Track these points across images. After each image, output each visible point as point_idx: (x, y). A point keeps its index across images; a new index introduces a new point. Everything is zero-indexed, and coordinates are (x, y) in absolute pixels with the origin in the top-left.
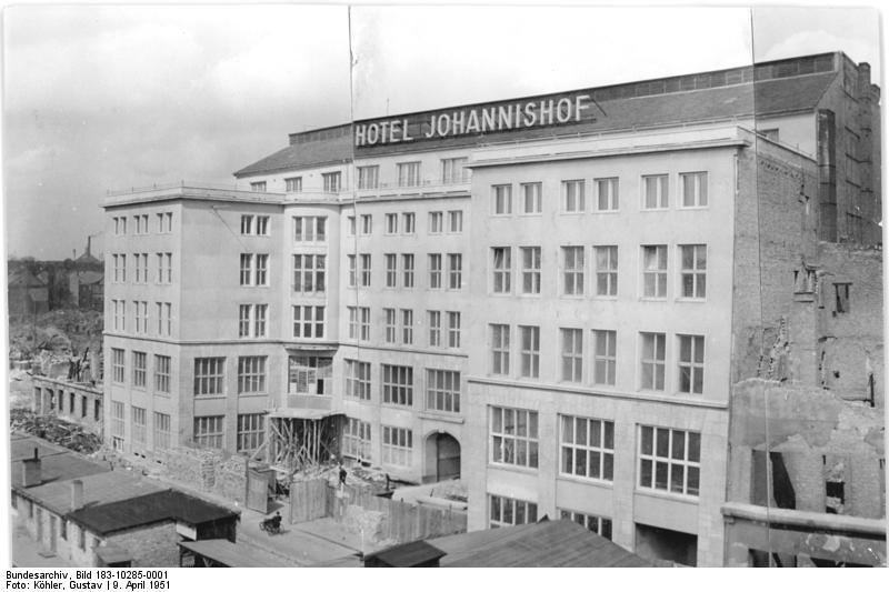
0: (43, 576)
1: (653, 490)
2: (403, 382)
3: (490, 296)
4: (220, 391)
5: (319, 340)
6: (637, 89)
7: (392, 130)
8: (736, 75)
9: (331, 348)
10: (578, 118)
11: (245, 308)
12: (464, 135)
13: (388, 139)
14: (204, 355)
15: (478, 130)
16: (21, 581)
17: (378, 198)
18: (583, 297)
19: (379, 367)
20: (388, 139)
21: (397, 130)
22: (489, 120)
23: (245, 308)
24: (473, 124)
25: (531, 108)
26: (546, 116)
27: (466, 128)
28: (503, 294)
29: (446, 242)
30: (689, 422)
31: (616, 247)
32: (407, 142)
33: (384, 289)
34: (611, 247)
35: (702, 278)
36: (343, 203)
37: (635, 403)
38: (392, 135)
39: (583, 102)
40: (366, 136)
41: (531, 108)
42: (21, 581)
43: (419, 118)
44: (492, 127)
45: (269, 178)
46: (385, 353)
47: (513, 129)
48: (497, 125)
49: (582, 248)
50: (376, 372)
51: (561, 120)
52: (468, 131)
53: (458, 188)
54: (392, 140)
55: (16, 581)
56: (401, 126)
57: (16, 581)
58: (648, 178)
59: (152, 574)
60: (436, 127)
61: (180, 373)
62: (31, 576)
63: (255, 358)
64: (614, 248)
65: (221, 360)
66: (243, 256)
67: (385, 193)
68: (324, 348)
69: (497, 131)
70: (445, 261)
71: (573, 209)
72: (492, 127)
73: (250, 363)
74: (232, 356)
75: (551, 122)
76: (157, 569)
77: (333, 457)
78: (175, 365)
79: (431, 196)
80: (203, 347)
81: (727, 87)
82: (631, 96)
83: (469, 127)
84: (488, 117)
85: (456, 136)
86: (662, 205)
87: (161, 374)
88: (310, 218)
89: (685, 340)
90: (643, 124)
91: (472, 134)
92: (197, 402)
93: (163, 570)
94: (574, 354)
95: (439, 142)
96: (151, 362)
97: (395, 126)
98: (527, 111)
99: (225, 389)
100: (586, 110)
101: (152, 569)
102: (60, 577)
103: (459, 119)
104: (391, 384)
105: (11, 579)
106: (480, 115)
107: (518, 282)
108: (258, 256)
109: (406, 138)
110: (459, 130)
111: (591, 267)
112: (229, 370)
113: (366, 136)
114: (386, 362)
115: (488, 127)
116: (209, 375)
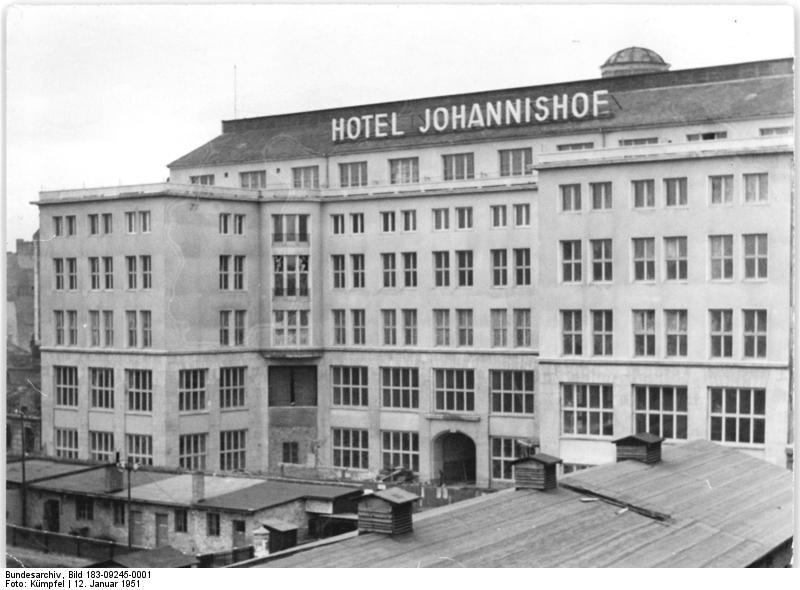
0: (39, 576)
1: (723, 443)
2: (144, 387)
3: (591, 285)
4: (203, 407)
5: (304, 347)
6: (741, 72)
7: (378, 124)
8: (751, 70)
9: (316, 355)
10: (596, 113)
11: (225, 313)
12: (467, 131)
13: (373, 132)
14: (188, 367)
15: (482, 124)
16: (19, 580)
17: (480, 189)
18: (655, 281)
19: (377, 371)
20: (373, 132)
21: (385, 124)
22: (494, 112)
23: (225, 313)
24: (476, 118)
25: (542, 103)
26: (560, 111)
27: (467, 124)
28: (573, 283)
29: (509, 237)
30: (753, 381)
31: (685, 238)
32: (396, 137)
33: (380, 291)
34: (725, 236)
35: (609, 266)
36: (325, 200)
37: (706, 370)
38: (377, 130)
39: (601, 98)
40: (570, 108)
41: (542, 103)
42: (19, 580)
43: (411, 109)
44: (498, 121)
45: (218, 173)
46: (385, 357)
47: (523, 124)
48: (503, 120)
49: (652, 239)
50: (83, 375)
51: (350, 136)
52: (469, 126)
53: (406, 188)
54: (378, 134)
55: (14, 580)
56: (387, 120)
57: (14, 580)
58: (564, 187)
59: (136, 574)
60: (431, 119)
61: (166, 387)
62: (28, 575)
63: (235, 369)
64: (683, 239)
65: (203, 372)
66: (221, 257)
67: (429, 187)
68: (310, 356)
69: (504, 126)
70: (400, 261)
71: (674, 203)
72: (498, 121)
73: (233, 376)
74: (214, 366)
75: (565, 116)
76: (141, 570)
77: (27, 454)
78: (159, 381)
79: (491, 190)
80: (186, 358)
81: (743, 80)
82: (639, 88)
83: (471, 122)
84: (512, 108)
85: (455, 131)
86: (681, 203)
87: (134, 390)
88: (290, 216)
89: (749, 314)
90: (758, 115)
91: (475, 129)
92: (91, 414)
93: (147, 570)
94: (722, 333)
95: (435, 138)
96: (121, 381)
97: (381, 120)
98: (539, 106)
99: (209, 403)
100: (603, 105)
101: (136, 570)
102: (54, 576)
103: (459, 112)
104: (98, 388)
105: (10, 579)
106: (484, 109)
107: (454, 278)
108: (236, 257)
109: (395, 132)
110: (459, 125)
111: (661, 256)
112: (212, 381)
113: (570, 108)
114: (385, 365)
115: (493, 121)
116: (232, 387)
